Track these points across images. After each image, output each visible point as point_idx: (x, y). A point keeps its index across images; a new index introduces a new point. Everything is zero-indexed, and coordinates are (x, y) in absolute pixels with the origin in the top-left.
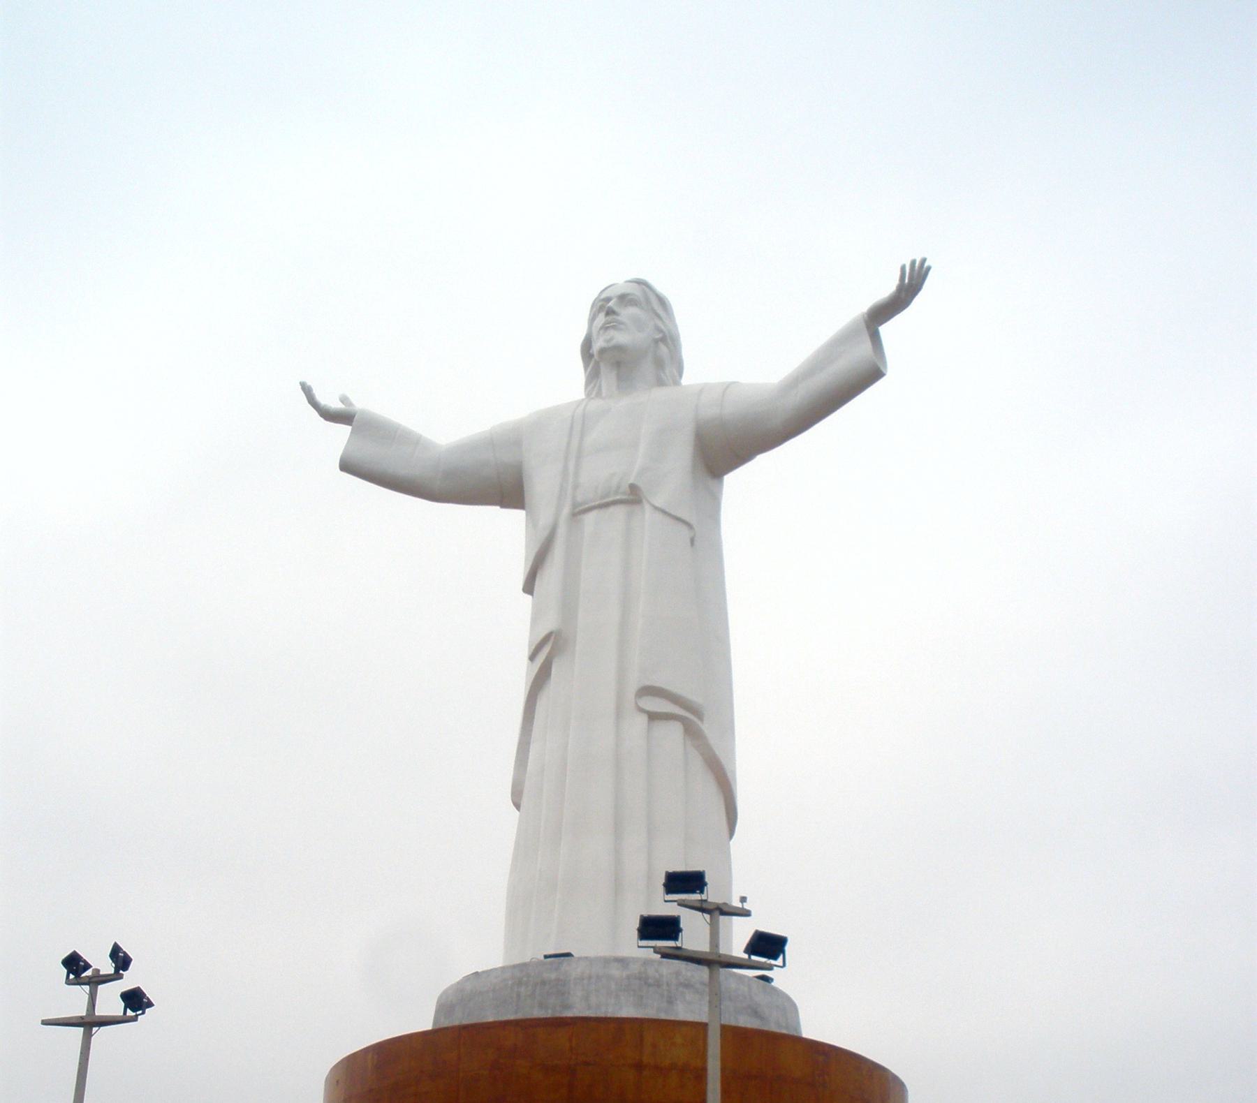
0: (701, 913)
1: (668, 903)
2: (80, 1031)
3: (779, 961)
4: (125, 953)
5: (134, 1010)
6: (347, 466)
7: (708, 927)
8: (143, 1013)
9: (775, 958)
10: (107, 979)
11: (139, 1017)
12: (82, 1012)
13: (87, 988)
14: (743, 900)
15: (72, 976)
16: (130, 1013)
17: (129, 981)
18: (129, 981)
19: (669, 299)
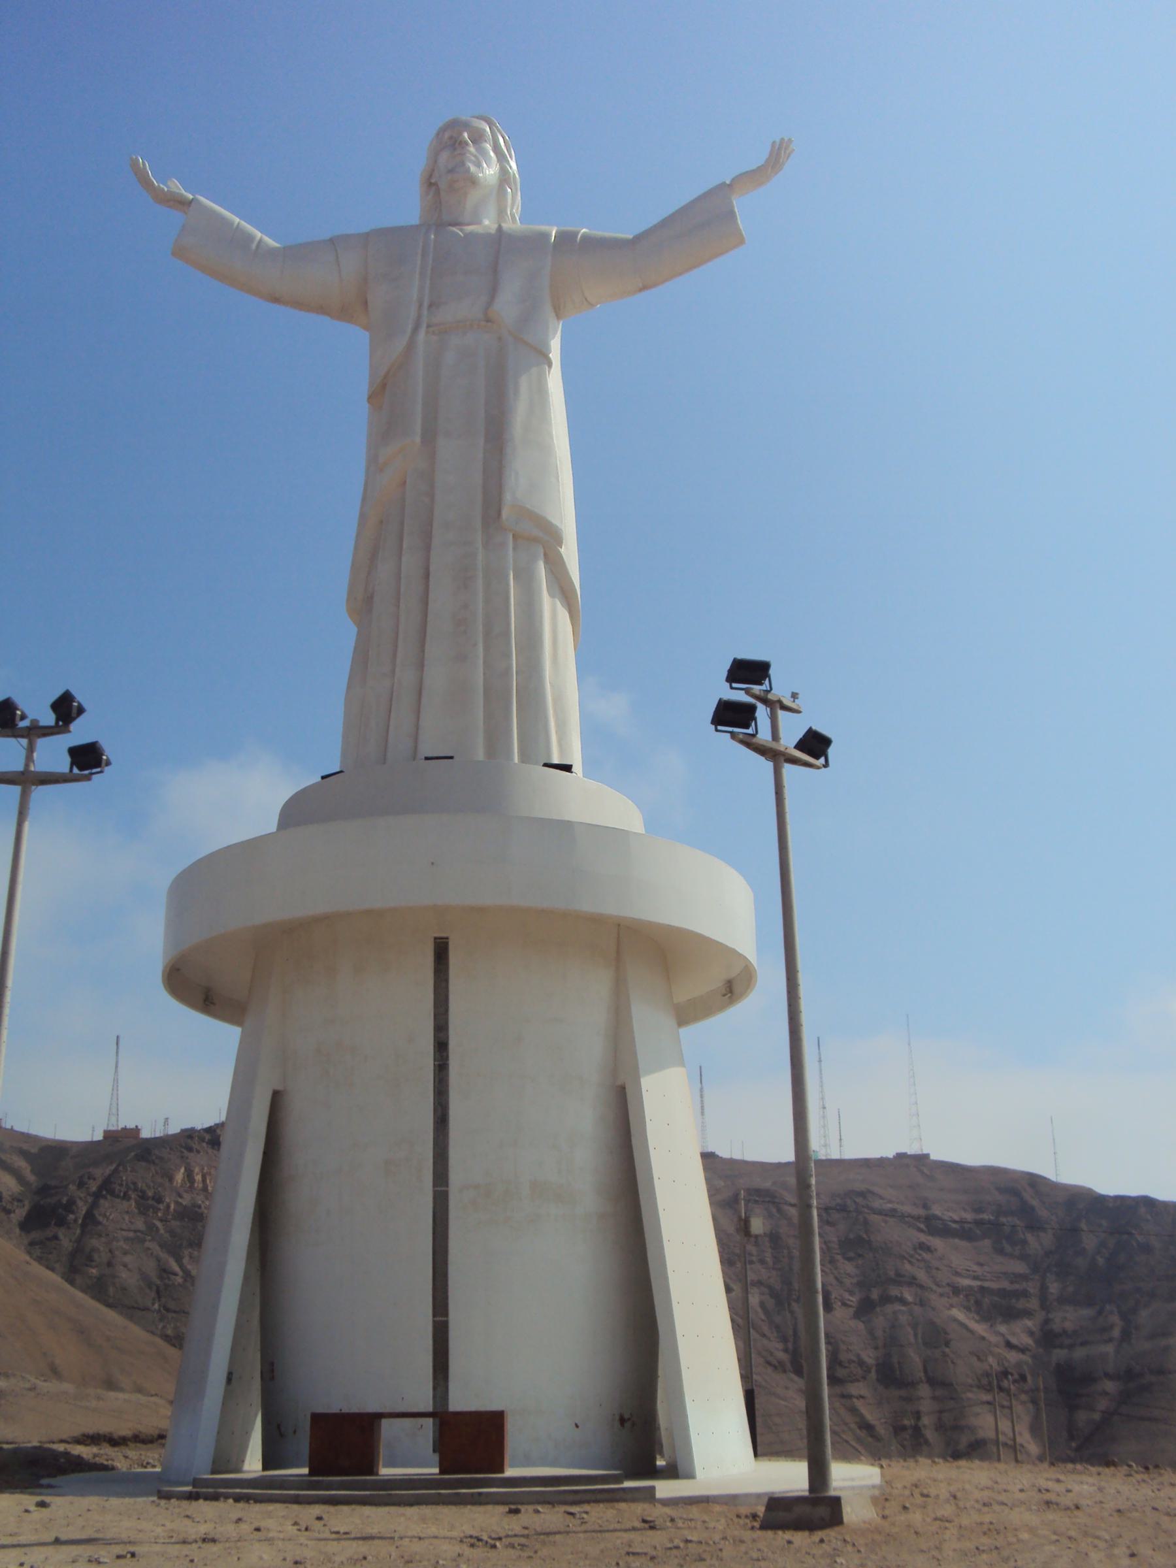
0: (764, 707)
1: (430, 761)
2: (16, 790)
3: (822, 760)
4: (79, 703)
5: (81, 769)
6: (179, 252)
7: (769, 720)
8: (101, 772)
9: (817, 757)
10: (47, 732)
11: (94, 777)
12: (20, 767)
13: (24, 742)
14: (794, 696)
15: (61, 723)
16: (76, 770)
17: (80, 733)
18: (80, 733)
19: (447, 120)
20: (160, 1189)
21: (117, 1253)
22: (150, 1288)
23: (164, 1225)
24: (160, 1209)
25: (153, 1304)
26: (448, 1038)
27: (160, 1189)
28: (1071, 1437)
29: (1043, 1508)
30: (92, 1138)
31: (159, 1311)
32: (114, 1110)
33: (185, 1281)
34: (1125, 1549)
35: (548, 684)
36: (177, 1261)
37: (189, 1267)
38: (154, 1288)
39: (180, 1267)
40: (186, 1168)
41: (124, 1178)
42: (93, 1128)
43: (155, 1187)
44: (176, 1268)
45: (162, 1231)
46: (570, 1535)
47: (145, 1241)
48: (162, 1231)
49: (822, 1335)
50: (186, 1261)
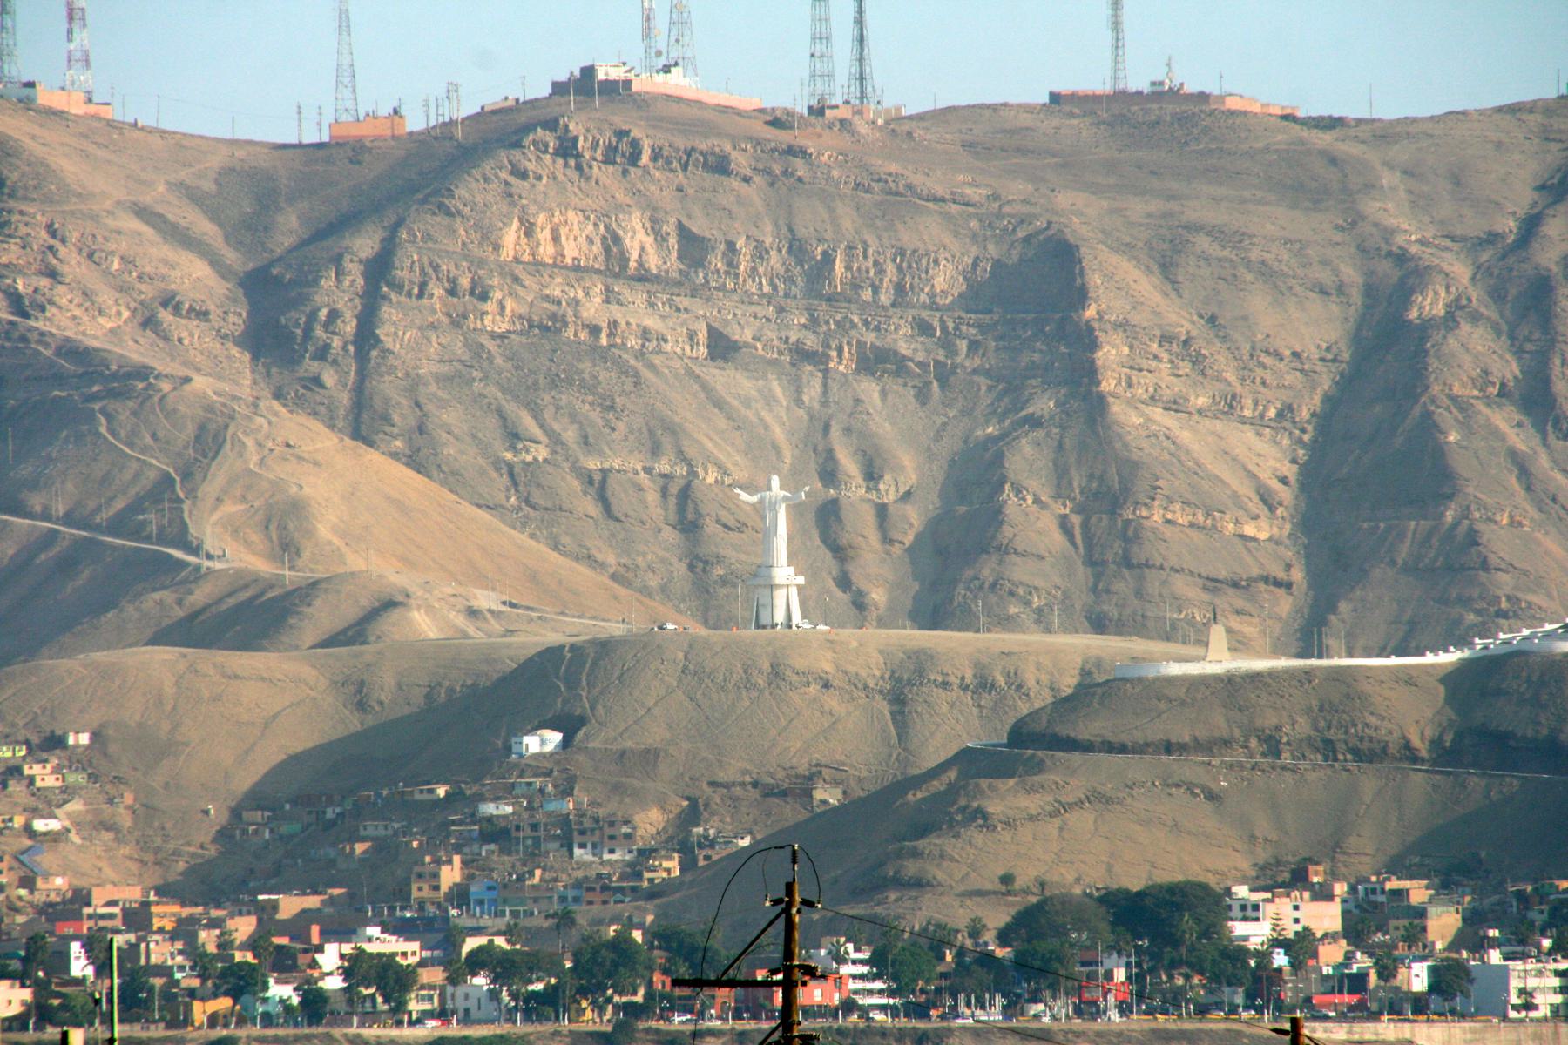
20: (481, 272)
21: (429, 407)
22: (498, 470)
23: (499, 346)
24: (486, 313)
25: (508, 498)
26: (1109, 634)
27: (481, 272)
28: (480, 395)
29: (749, 413)
30: (300, 135)
31: (519, 509)
32: (347, 76)
33: (554, 452)
34: (83, 95)
35: (1085, 641)
36: (535, 417)
37: (557, 427)
38: (505, 470)
39: (541, 426)
40: (520, 220)
41: (415, 257)
42: (299, 107)
43: (473, 269)
44: (537, 432)
45: (499, 360)
46: (1022, 198)
47: (474, 380)
48: (499, 360)
49: (1394, 661)
50: (548, 414)
